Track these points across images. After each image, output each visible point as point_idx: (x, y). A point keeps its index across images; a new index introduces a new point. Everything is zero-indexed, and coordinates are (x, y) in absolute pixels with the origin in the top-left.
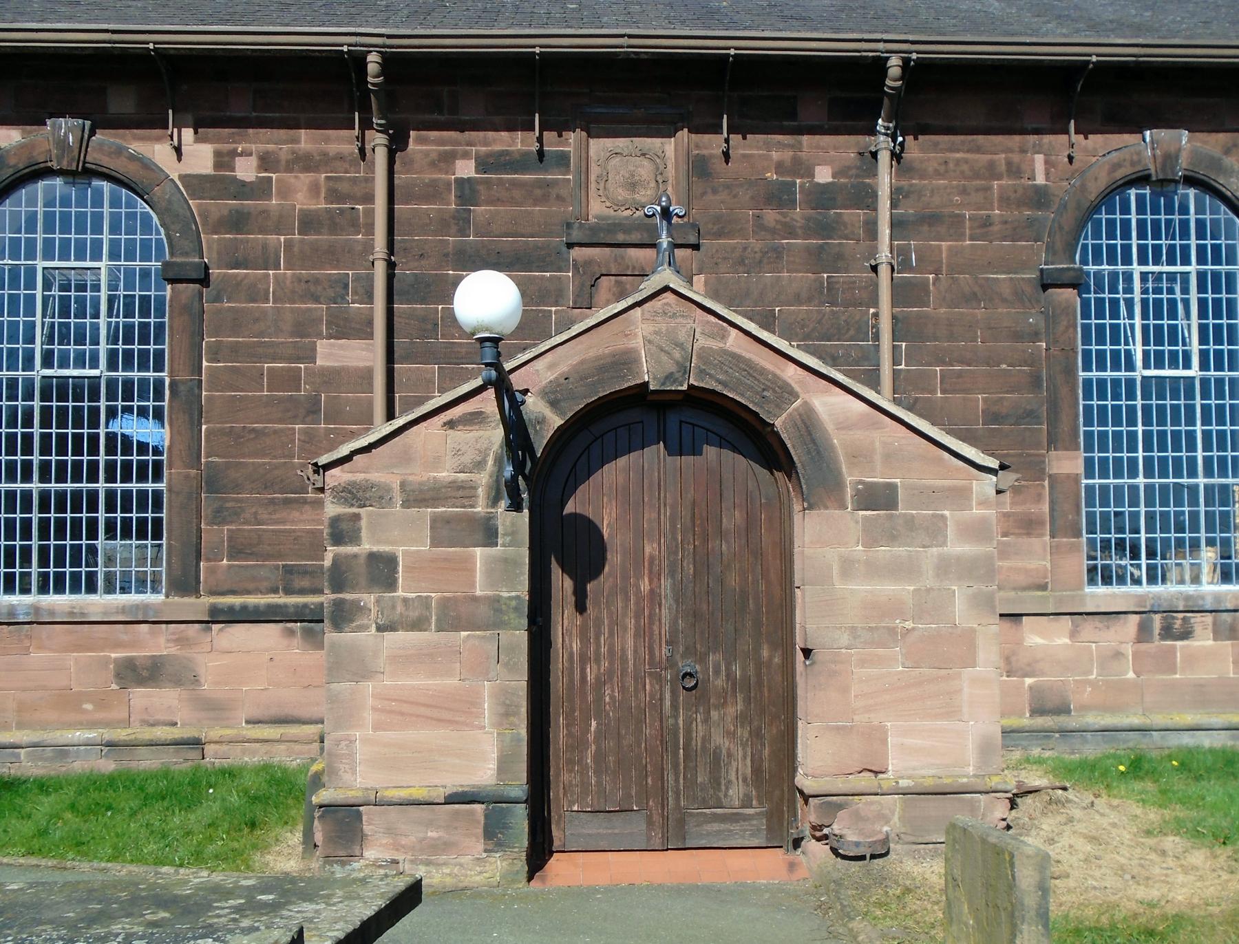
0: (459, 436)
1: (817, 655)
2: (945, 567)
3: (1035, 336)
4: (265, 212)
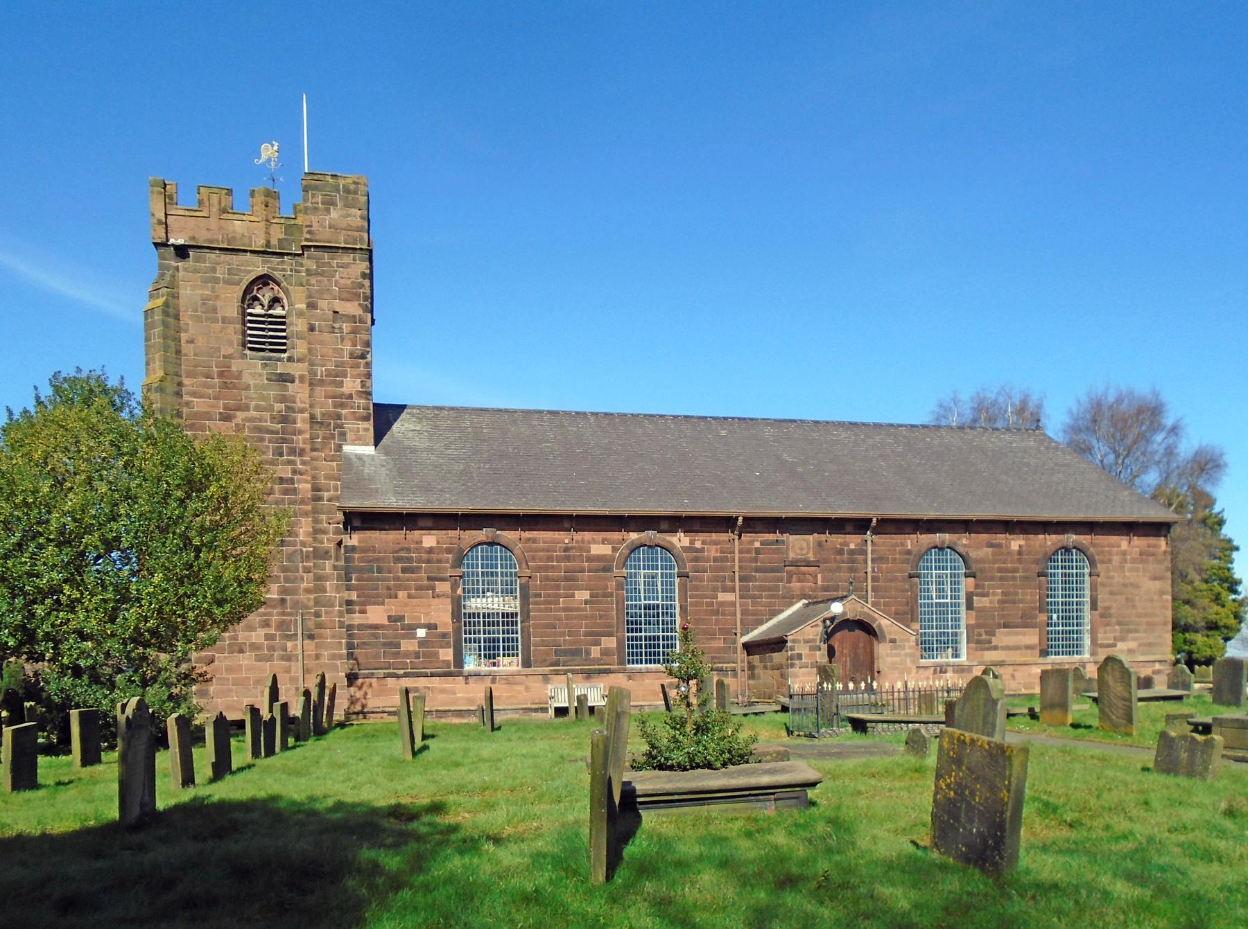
0: (813, 629)
1: (882, 672)
2: (906, 655)
3: (907, 591)
4: (703, 557)
